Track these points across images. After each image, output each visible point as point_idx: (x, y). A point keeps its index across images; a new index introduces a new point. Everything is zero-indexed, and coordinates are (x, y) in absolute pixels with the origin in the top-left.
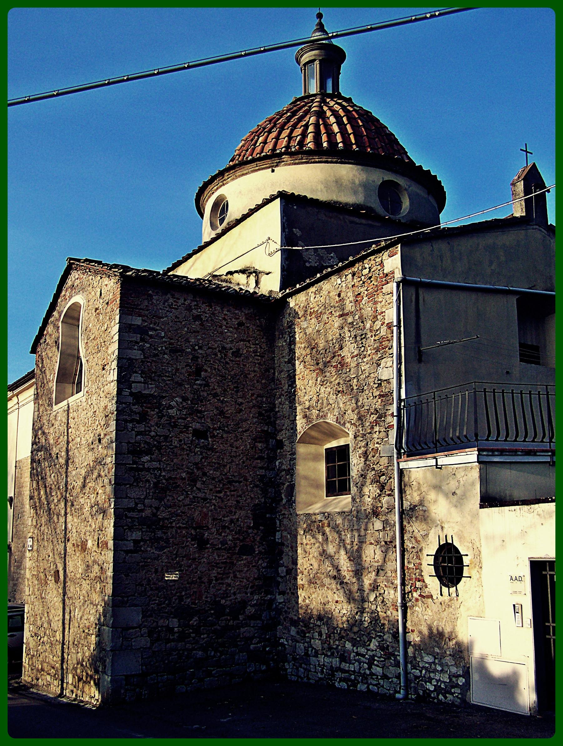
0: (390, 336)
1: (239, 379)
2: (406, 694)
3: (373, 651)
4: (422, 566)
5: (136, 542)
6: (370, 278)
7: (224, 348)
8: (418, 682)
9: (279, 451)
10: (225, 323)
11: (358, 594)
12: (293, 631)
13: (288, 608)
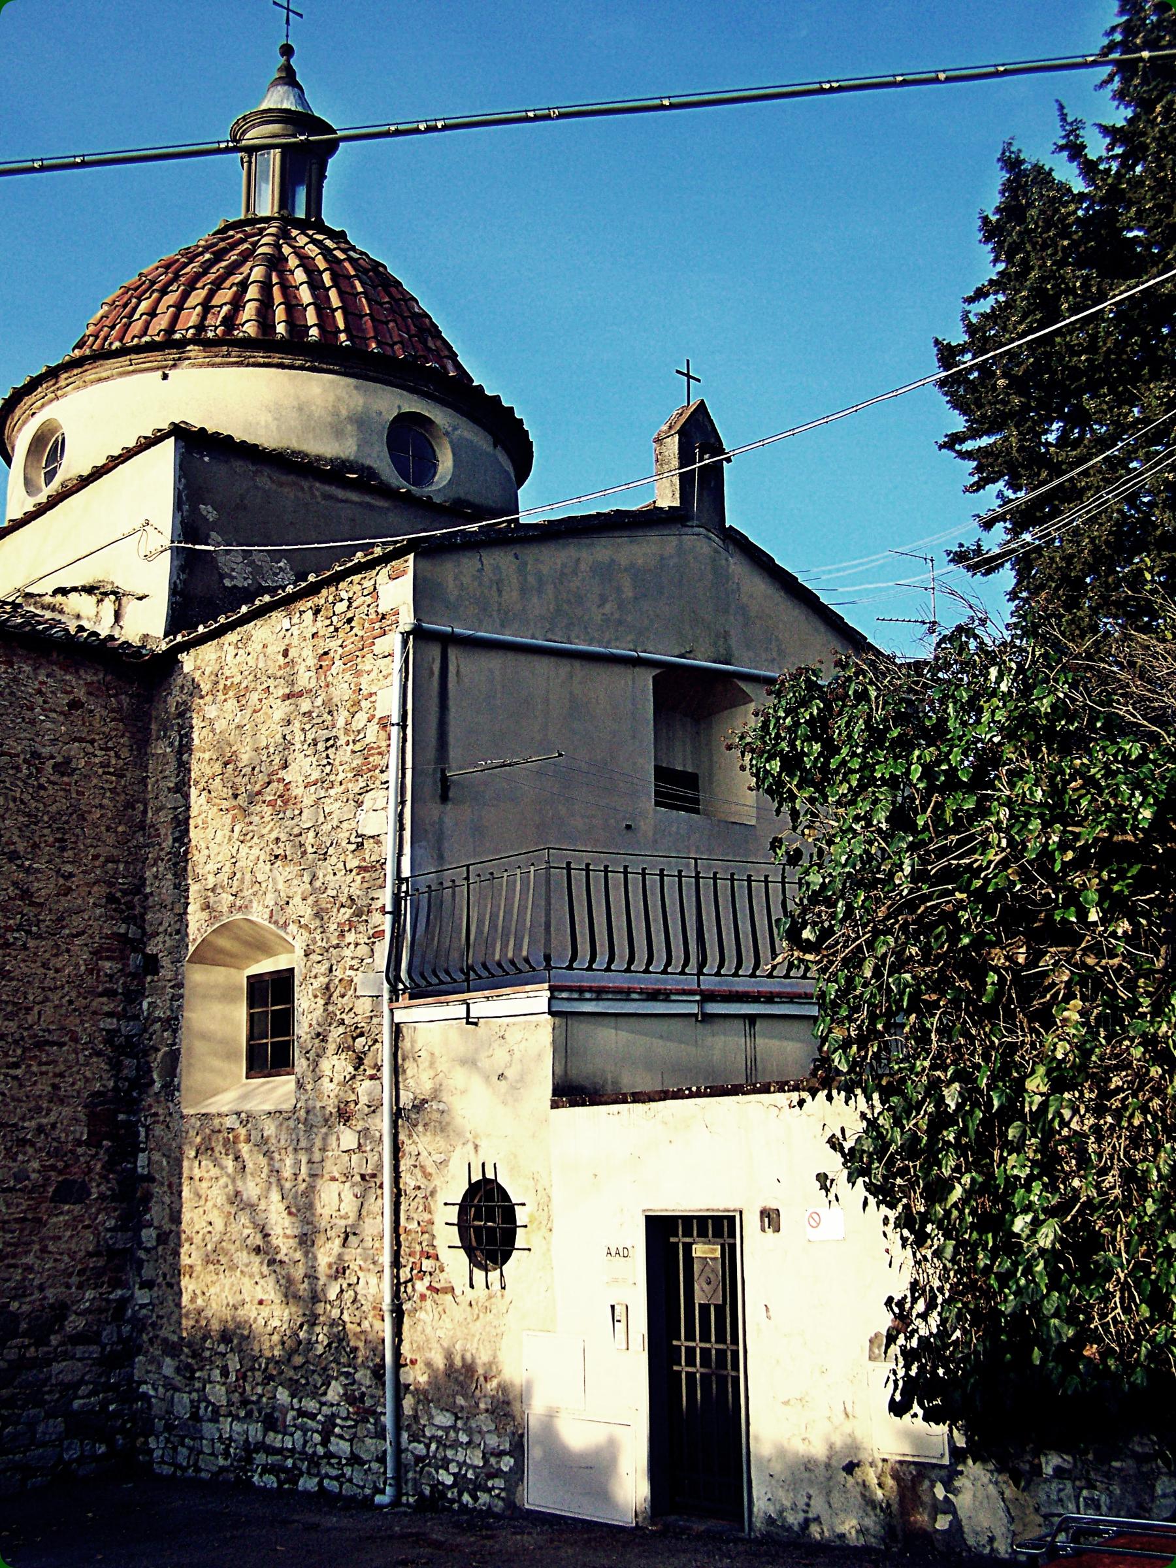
0: (384, 744)
1: (67, 822)
2: (399, 1494)
3: (332, 1405)
4: (435, 1227)
6: (350, 621)
7: (36, 755)
8: (422, 1469)
9: (149, 979)
11: (305, 1285)
12: (169, 1367)
13: (160, 1317)
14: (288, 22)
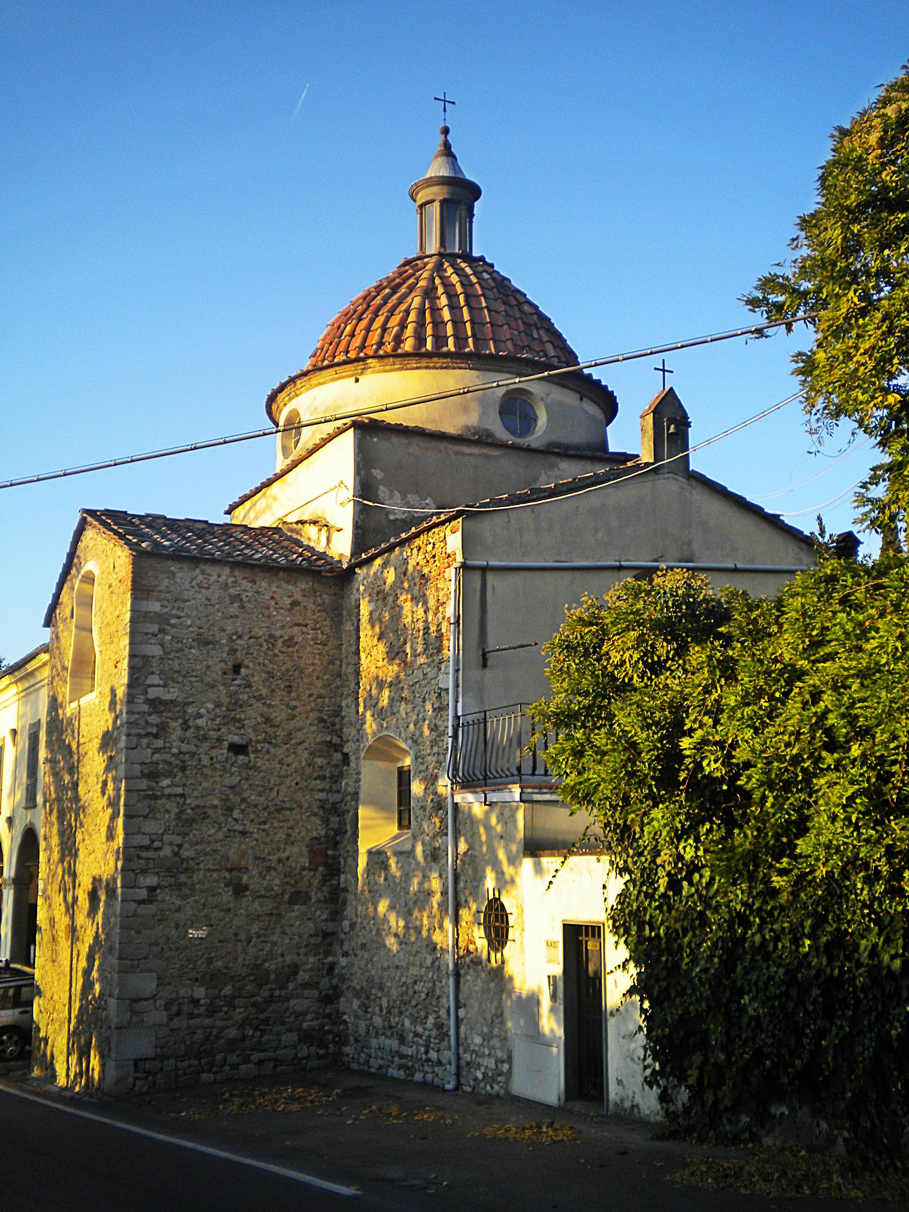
5: (152, 889)
6: (434, 556)
7: (271, 636)
10: (273, 603)
12: (356, 1003)
13: (351, 974)
14: (445, 110)
